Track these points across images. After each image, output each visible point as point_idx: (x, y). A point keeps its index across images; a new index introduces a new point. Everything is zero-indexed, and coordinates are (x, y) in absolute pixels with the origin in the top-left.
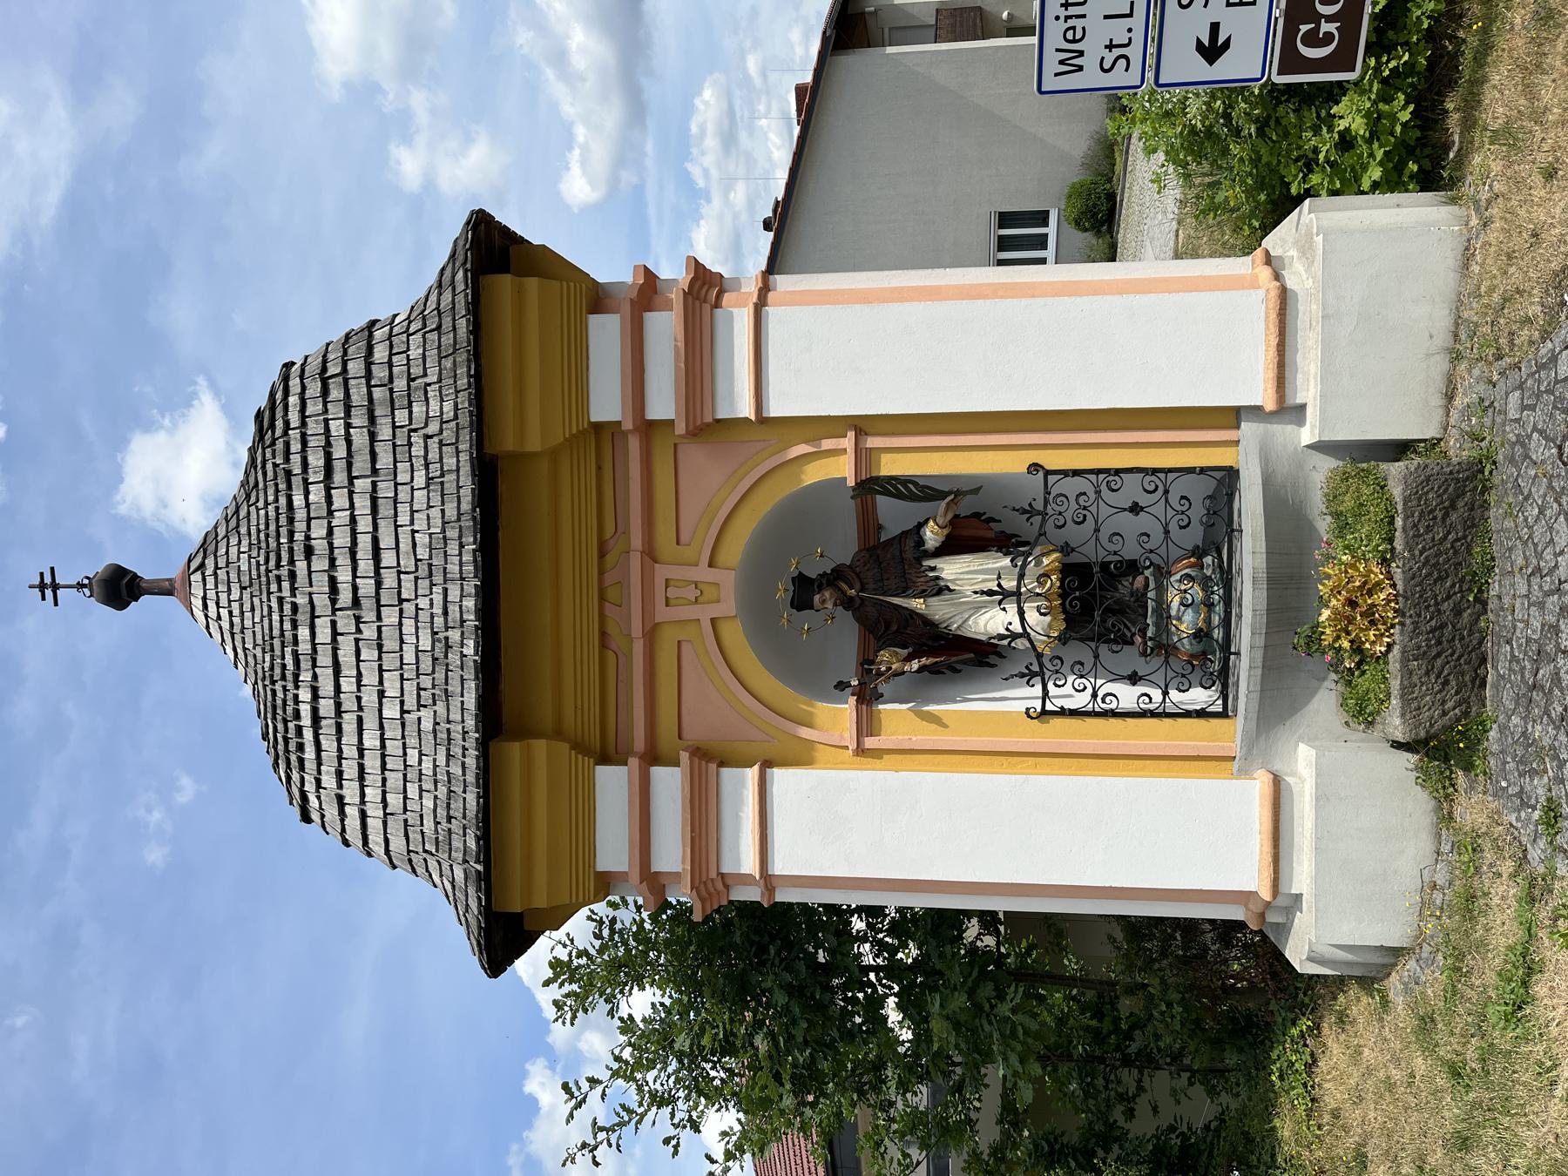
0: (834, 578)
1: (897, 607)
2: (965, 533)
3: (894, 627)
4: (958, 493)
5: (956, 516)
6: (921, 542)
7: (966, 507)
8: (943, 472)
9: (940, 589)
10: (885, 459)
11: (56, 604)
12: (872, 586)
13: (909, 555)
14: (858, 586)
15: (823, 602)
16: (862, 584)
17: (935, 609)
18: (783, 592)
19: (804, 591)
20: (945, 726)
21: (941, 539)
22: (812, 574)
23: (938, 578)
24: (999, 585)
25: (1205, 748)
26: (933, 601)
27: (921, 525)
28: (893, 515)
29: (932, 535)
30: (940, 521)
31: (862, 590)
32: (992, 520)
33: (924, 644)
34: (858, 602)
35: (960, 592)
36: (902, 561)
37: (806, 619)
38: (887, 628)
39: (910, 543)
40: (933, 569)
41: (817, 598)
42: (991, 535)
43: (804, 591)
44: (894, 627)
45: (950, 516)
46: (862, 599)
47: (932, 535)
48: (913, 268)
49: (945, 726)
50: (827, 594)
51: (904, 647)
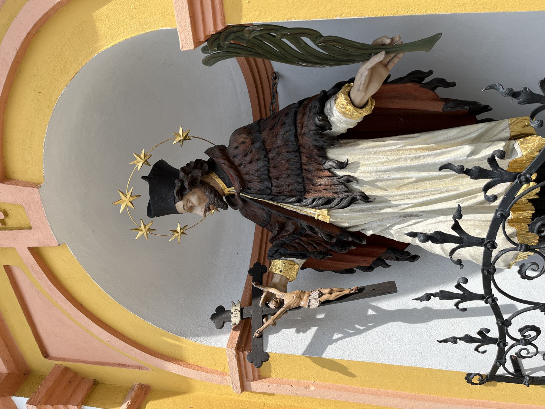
0: (217, 161)
2: (397, 105)
7: (403, 64)
8: (367, 14)
9: (350, 194)
13: (308, 140)
14: (237, 183)
18: (133, 196)
19: (166, 186)
20: (352, 375)
22: (178, 162)
23: (349, 179)
24: (456, 227)
27: (325, 97)
29: (341, 115)
30: (358, 96)
31: (242, 191)
32: (443, 83)
35: (383, 201)
40: (342, 165)
42: (438, 108)
43: (166, 186)
45: (374, 88)
47: (341, 115)
48: (432, 370)
49: (352, 375)
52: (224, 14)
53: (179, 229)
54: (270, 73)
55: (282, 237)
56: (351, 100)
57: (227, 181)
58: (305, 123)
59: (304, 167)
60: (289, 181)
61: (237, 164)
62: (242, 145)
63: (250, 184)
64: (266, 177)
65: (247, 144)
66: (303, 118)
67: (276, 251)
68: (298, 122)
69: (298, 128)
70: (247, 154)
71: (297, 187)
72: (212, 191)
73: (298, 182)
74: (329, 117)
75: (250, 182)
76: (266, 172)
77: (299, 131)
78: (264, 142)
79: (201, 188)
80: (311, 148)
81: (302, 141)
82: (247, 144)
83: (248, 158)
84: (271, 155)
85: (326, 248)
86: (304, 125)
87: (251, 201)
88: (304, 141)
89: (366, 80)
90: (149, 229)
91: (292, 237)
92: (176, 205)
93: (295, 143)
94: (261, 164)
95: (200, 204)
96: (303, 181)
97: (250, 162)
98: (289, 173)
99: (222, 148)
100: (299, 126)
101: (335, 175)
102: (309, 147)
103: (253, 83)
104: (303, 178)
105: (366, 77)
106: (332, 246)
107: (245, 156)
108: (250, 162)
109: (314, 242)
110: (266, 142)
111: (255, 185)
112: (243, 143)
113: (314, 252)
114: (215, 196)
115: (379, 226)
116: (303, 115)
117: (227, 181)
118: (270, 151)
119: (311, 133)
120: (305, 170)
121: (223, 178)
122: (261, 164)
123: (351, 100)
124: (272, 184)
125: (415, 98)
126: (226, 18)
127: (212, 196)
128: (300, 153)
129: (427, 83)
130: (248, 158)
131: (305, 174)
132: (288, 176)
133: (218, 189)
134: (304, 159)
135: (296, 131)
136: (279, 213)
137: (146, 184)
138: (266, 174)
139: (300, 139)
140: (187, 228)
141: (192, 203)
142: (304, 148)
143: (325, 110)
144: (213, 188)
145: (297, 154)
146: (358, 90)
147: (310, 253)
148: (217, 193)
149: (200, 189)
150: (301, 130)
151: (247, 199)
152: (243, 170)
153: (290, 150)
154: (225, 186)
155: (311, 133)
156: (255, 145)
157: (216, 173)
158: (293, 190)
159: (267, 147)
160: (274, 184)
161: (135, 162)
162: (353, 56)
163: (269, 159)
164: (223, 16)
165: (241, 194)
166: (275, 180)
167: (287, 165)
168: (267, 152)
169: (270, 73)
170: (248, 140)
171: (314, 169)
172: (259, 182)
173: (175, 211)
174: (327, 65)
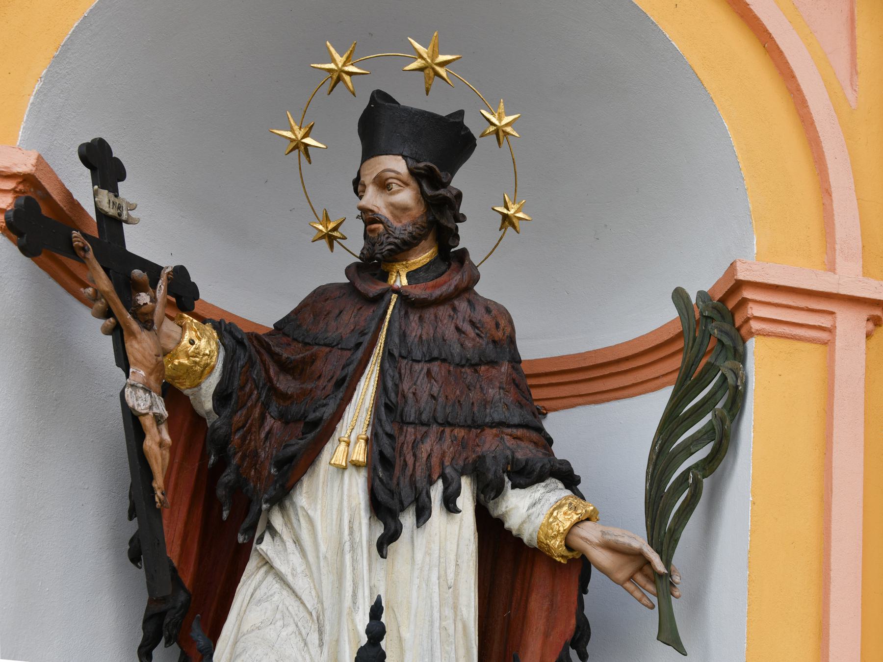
1: (345, 387)
3: (285, 384)
4: (664, 584)
5: (581, 567)
6: (526, 476)
9: (392, 504)
10: (808, 357)
11: (310, 162)
12: (415, 329)
13: (490, 444)
14: (418, 292)
15: (383, 184)
16: (421, 305)
17: (333, 496)
21: (529, 535)
23: (423, 515)
25: (575, 393)
26: (356, 487)
28: (613, 441)
29: (530, 510)
30: (590, 533)
33: (222, 464)
34: (373, 289)
36: (476, 425)
37: (337, 141)
38: (285, 367)
39: (525, 452)
40: (450, 505)
41: (396, 165)
44: (285, 384)
46: (380, 299)
47: (530, 510)
50: (406, 196)
51: (221, 396)
52: (769, 336)
53: (308, 141)
54: (546, 404)
55: (263, 362)
56: (582, 521)
57: (422, 274)
58: (522, 444)
59: (448, 430)
60: (424, 397)
61: (456, 303)
62: (494, 323)
63: (416, 318)
64: (435, 354)
65: (494, 331)
66: (531, 441)
67: (240, 343)
68: (525, 431)
69: (515, 430)
70: (478, 328)
71: (413, 411)
72: (414, 238)
73: (421, 414)
74: (543, 484)
75: (421, 319)
76: (444, 356)
77: (509, 431)
78: (493, 363)
79: (424, 219)
80: (478, 449)
81: (489, 433)
82: (494, 331)
83: (467, 327)
84: (467, 370)
85: (235, 454)
86: (519, 442)
87: (381, 311)
88: (489, 439)
89: (624, 544)
90: (339, 79)
91: (264, 385)
92: (400, 158)
93: (487, 420)
94: (456, 349)
95: (394, 207)
96: (423, 424)
97: (458, 329)
98: (440, 400)
99: (475, 279)
100: (519, 432)
101: (431, 482)
102: (478, 446)
103: (536, 372)
104: (427, 425)
105: (629, 545)
106: (239, 467)
107: (472, 323)
108: (458, 329)
109: (249, 431)
110: (494, 368)
111: (415, 329)
112: (497, 325)
113: (230, 425)
114: (404, 242)
115: (293, 569)
116: (535, 443)
117: (422, 274)
118: (476, 371)
119: (508, 453)
120: (443, 432)
121: (428, 268)
122: (456, 349)
123: (582, 521)
124: (418, 361)
125: (546, 635)
126: (762, 337)
127: (406, 237)
128: (469, 427)
129: (568, 653)
130: (467, 327)
131: (435, 428)
132: (433, 397)
133: (411, 252)
134: (460, 433)
135: (509, 426)
136: (355, 363)
137: (443, 110)
138: (440, 354)
139: (494, 431)
140: (303, 157)
141: (398, 192)
142: (477, 436)
143: (554, 480)
144: (417, 245)
145: (469, 422)
146: (603, 533)
147: (231, 417)
148: (403, 248)
149: (422, 216)
150: (511, 435)
151: (383, 305)
152: (443, 311)
153: (476, 409)
154: (414, 268)
155: (508, 453)
156: (491, 346)
157: (435, 259)
158: (406, 402)
159: (483, 368)
160: (417, 367)
161: (502, 108)
162: (660, 529)
163: (463, 366)
164: (768, 335)
165: (394, 297)
166: (425, 370)
167: (451, 397)
168: (474, 366)
169: (546, 404)
170: (500, 334)
171: (445, 447)
172: (421, 337)
173: (370, 151)
174: (651, 485)
